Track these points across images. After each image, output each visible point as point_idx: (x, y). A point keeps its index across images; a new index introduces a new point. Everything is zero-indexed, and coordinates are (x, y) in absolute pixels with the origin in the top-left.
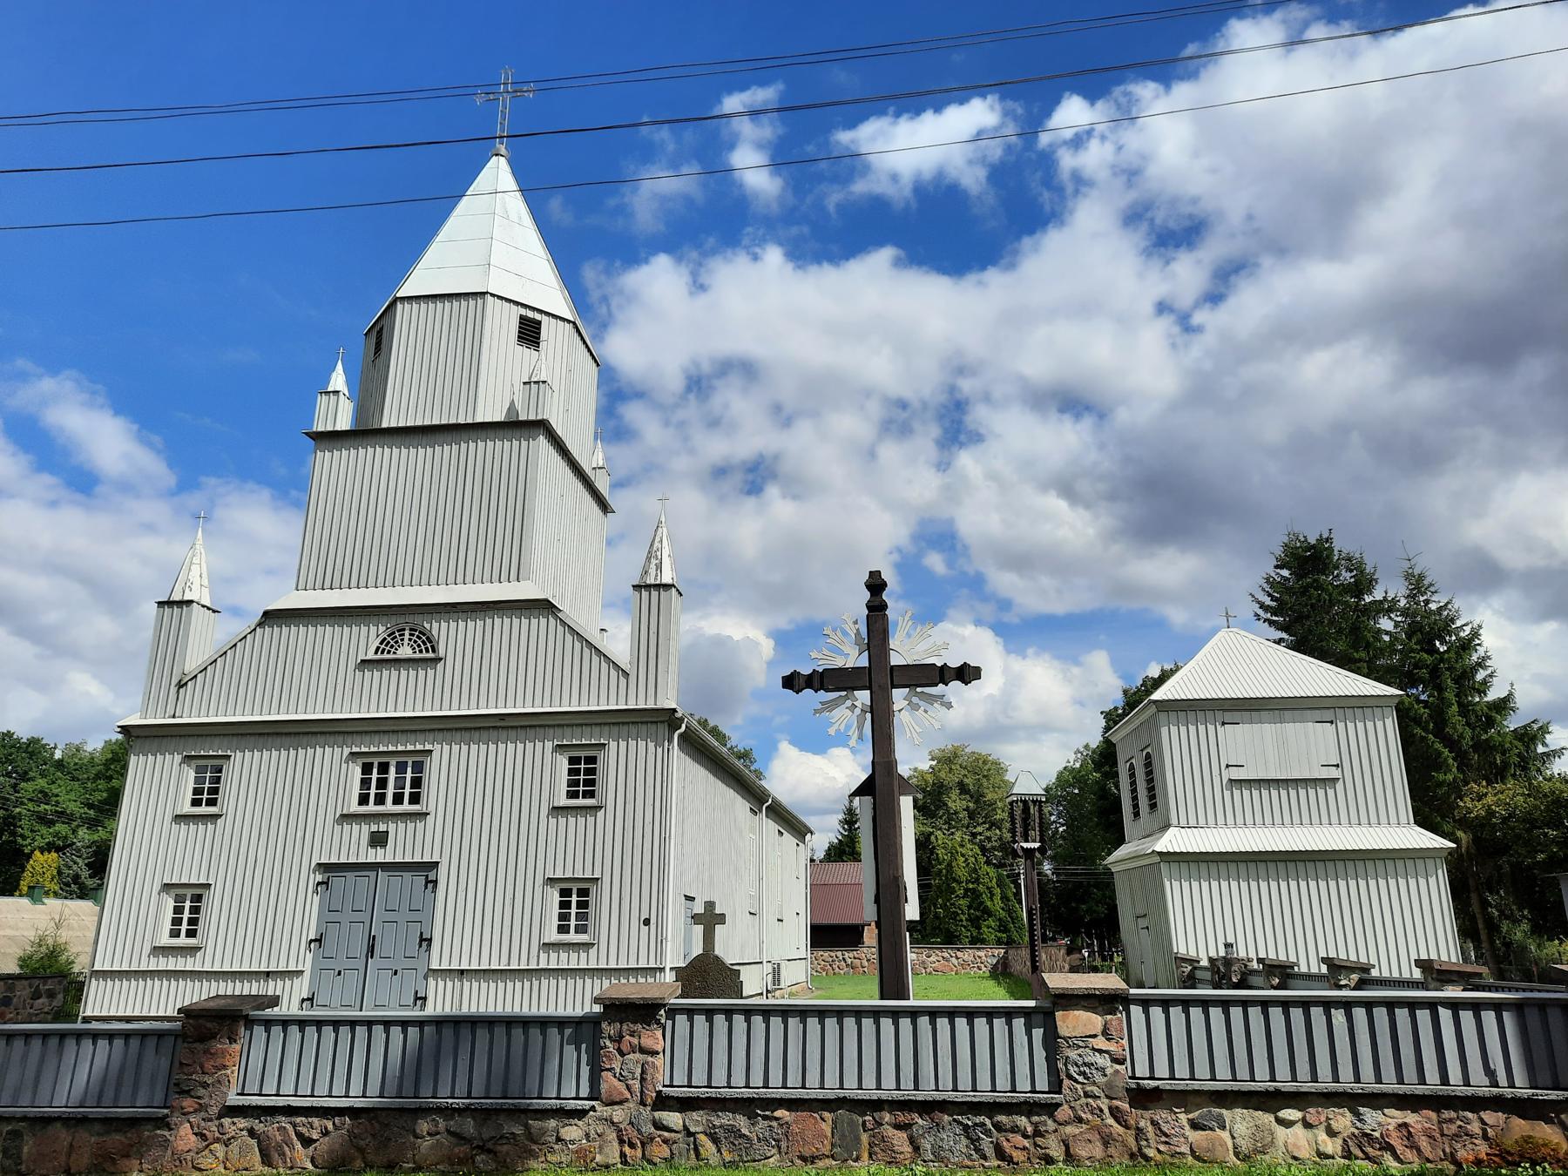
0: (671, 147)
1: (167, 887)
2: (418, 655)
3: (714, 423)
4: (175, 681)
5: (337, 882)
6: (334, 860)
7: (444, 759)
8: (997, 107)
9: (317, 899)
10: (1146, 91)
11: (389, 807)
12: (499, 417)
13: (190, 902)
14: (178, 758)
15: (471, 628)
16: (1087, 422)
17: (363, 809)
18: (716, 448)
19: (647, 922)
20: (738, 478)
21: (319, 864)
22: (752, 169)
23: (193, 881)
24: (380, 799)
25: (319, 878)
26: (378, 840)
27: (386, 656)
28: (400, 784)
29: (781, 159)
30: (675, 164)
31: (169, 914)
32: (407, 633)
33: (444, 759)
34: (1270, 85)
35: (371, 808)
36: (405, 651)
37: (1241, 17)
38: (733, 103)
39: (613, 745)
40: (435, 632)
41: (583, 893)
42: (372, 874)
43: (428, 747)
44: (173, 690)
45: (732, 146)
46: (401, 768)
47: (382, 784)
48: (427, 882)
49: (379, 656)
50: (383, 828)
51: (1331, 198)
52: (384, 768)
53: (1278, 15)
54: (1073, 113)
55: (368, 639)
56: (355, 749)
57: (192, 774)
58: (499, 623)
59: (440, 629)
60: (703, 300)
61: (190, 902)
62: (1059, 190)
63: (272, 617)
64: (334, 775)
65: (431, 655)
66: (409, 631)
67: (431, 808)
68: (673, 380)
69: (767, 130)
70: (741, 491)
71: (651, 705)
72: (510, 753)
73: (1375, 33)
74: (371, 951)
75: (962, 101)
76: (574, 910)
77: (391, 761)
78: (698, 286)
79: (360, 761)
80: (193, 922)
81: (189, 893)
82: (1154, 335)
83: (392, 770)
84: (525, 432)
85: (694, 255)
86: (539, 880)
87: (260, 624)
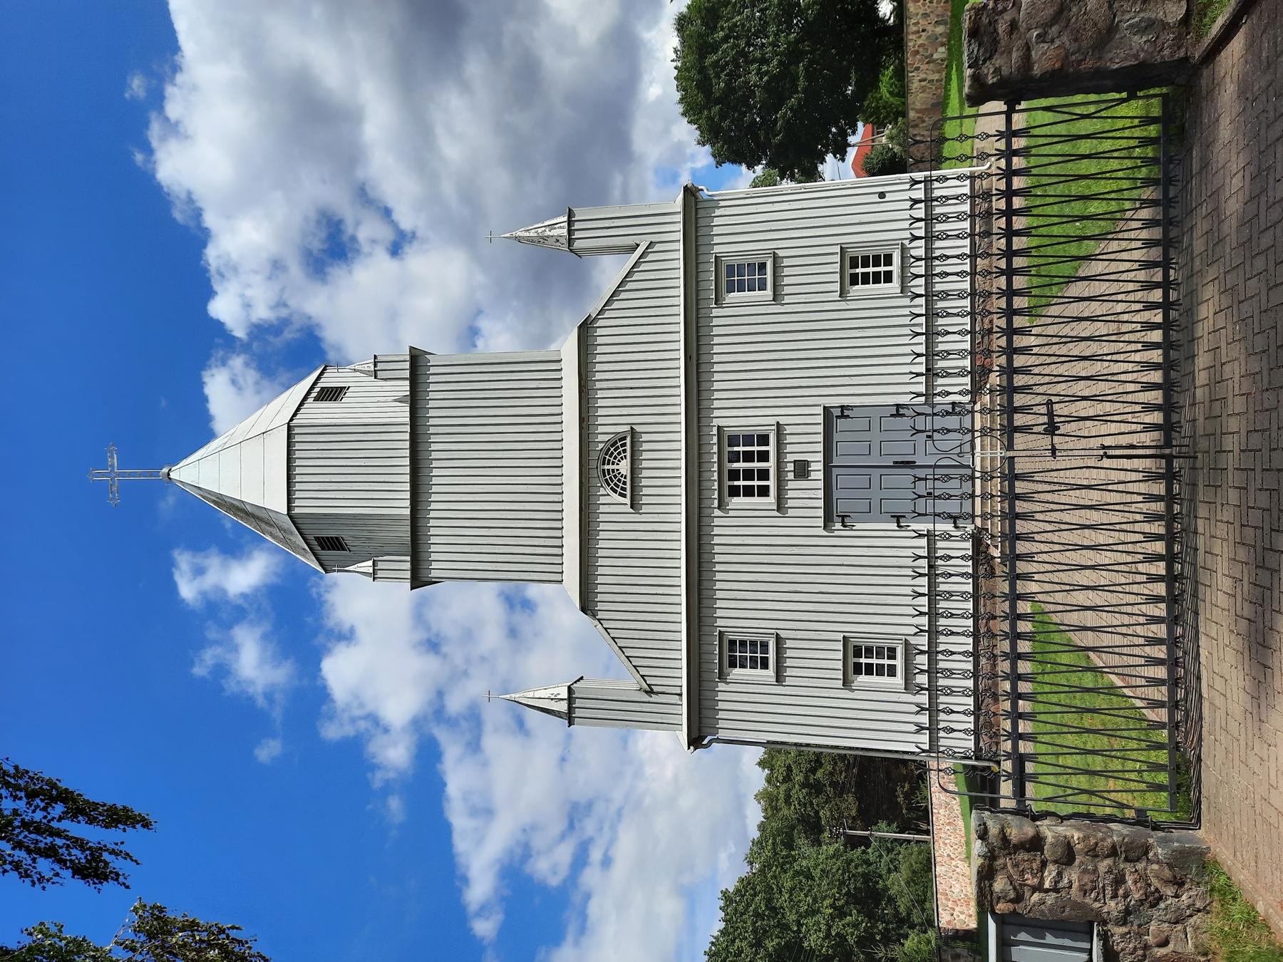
0: (219, 650)
1: (846, 683)
2: (628, 454)
3: (468, 635)
4: (646, 698)
5: (841, 507)
6: (821, 513)
7: (730, 414)
8: (214, 371)
9: (858, 526)
10: (212, 254)
11: (771, 465)
12: (405, 409)
13: (860, 659)
14: (722, 686)
15: (604, 400)
16: (484, 324)
17: (773, 491)
18: (492, 637)
19: (882, 195)
20: (519, 617)
21: (825, 528)
22: (245, 576)
23: (840, 655)
24: (764, 474)
25: (838, 526)
26: (802, 470)
27: (628, 487)
28: (748, 457)
29: (234, 548)
30: (235, 649)
31: (874, 679)
32: (606, 467)
33: (730, 414)
34: (208, 145)
35: (772, 483)
36: (624, 467)
37: (154, 171)
38: (187, 590)
39: (717, 249)
40: (606, 438)
41: (854, 263)
42: (835, 471)
43: (715, 431)
44: (655, 698)
45: (224, 592)
46: (735, 457)
47: (749, 474)
48: (843, 416)
49: (628, 493)
50: (791, 467)
51: (308, 119)
52: (734, 475)
53: (155, 143)
54: (224, 308)
55: (611, 502)
56: (716, 503)
57: (737, 671)
58: (601, 373)
59: (605, 430)
60: (362, 632)
61: (860, 659)
62: (284, 323)
63: (587, 605)
64: (740, 523)
65: (628, 441)
66: (607, 463)
67: (773, 421)
68: (431, 664)
69: (214, 562)
70: (530, 616)
71: (680, 218)
72: (721, 349)
73: (176, 69)
74: (909, 464)
75: (205, 400)
76: (871, 269)
77: (731, 467)
78: (347, 636)
79: (727, 499)
80: (880, 654)
81: (852, 660)
82: (417, 262)
83: (736, 465)
84: (421, 370)
85: (321, 639)
86: (843, 305)
87: (594, 616)
